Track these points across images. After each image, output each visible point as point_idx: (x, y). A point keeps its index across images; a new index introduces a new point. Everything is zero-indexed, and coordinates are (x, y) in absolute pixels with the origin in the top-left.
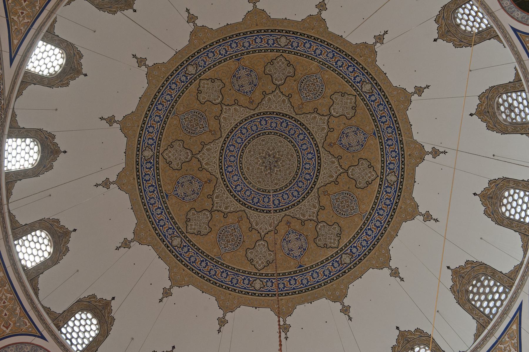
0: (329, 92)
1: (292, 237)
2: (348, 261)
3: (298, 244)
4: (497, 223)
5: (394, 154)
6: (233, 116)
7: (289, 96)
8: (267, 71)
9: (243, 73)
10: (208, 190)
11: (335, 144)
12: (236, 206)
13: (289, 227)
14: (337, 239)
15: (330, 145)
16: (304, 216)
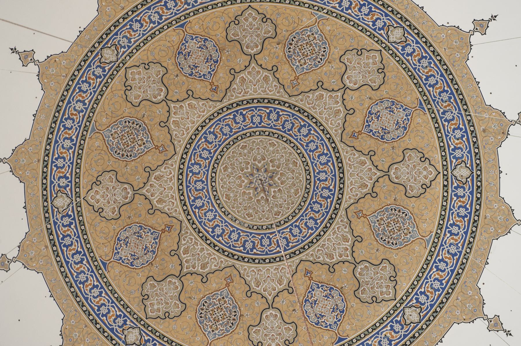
0: (336, 52)
1: (318, 294)
3: (330, 304)
7: (274, 70)
8: (231, 36)
9: (193, 45)
10: (168, 242)
11: (360, 133)
12: (217, 260)
13: (311, 279)
16: (331, 257)
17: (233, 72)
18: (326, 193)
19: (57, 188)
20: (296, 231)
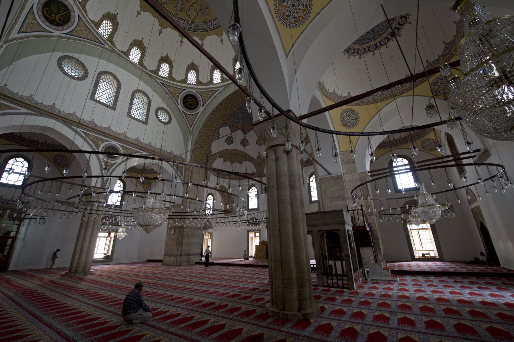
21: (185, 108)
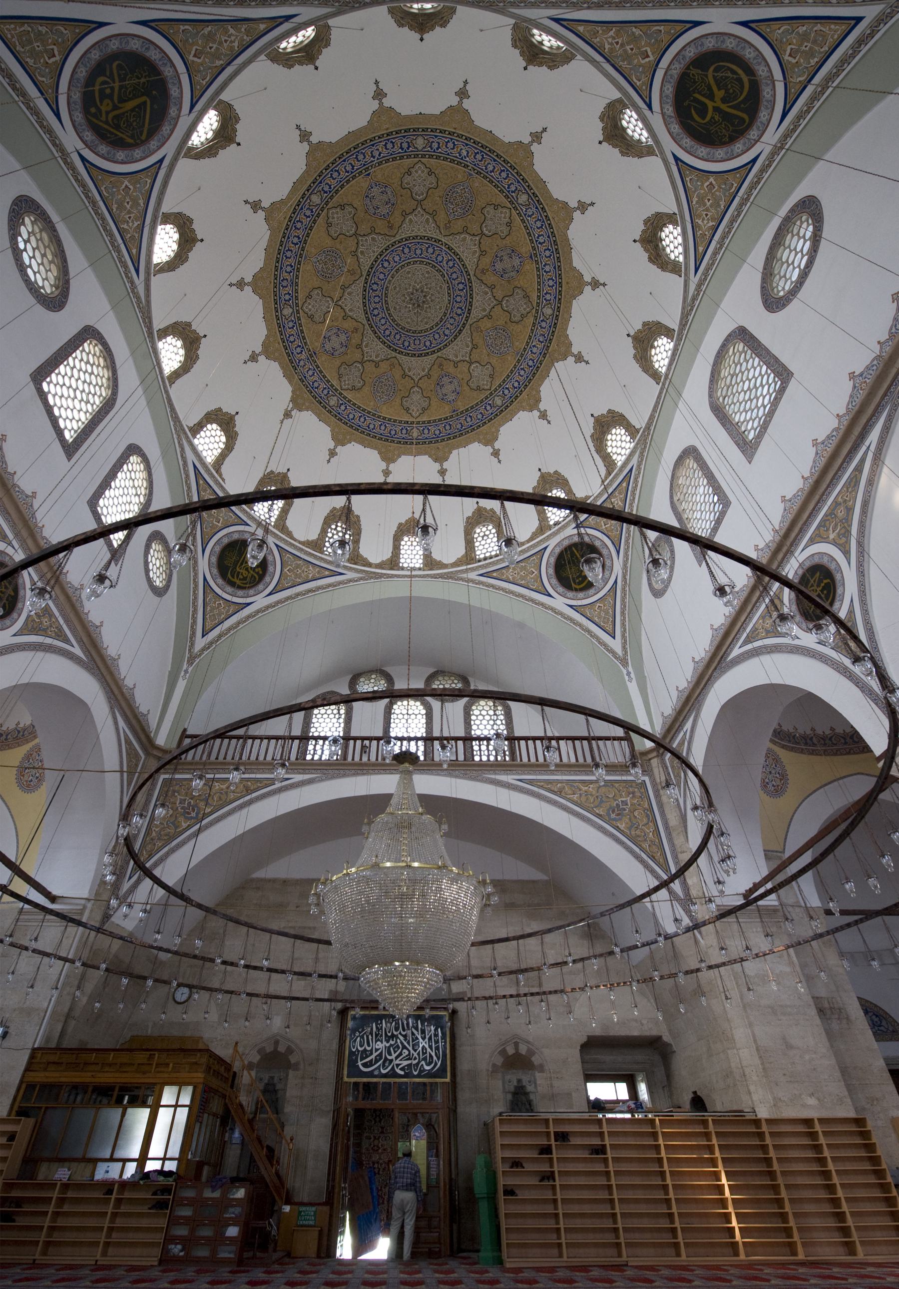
0: (494, 361)
1: (343, 337)
2: (332, 403)
3: (337, 346)
4: (395, 536)
5: (437, 432)
6: (467, 249)
7: (489, 316)
8: (517, 290)
9: (516, 262)
10: (381, 226)
11: (442, 370)
12: (366, 262)
13: (353, 332)
14: (350, 387)
15: (441, 365)
16: (366, 346)
17: (492, 287)
18: (406, 344)
19: (431, 140)
20: (383, 321)
21: (763, 115)
